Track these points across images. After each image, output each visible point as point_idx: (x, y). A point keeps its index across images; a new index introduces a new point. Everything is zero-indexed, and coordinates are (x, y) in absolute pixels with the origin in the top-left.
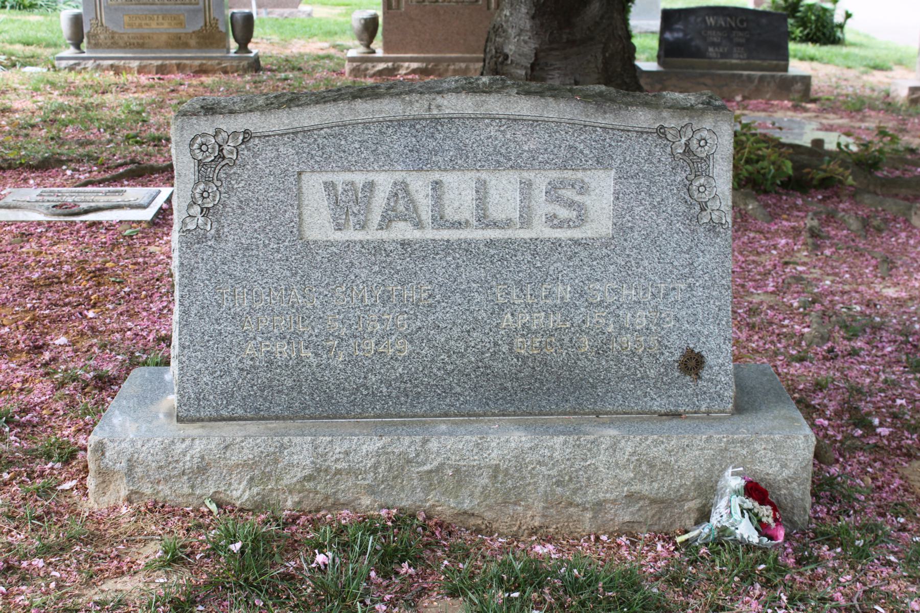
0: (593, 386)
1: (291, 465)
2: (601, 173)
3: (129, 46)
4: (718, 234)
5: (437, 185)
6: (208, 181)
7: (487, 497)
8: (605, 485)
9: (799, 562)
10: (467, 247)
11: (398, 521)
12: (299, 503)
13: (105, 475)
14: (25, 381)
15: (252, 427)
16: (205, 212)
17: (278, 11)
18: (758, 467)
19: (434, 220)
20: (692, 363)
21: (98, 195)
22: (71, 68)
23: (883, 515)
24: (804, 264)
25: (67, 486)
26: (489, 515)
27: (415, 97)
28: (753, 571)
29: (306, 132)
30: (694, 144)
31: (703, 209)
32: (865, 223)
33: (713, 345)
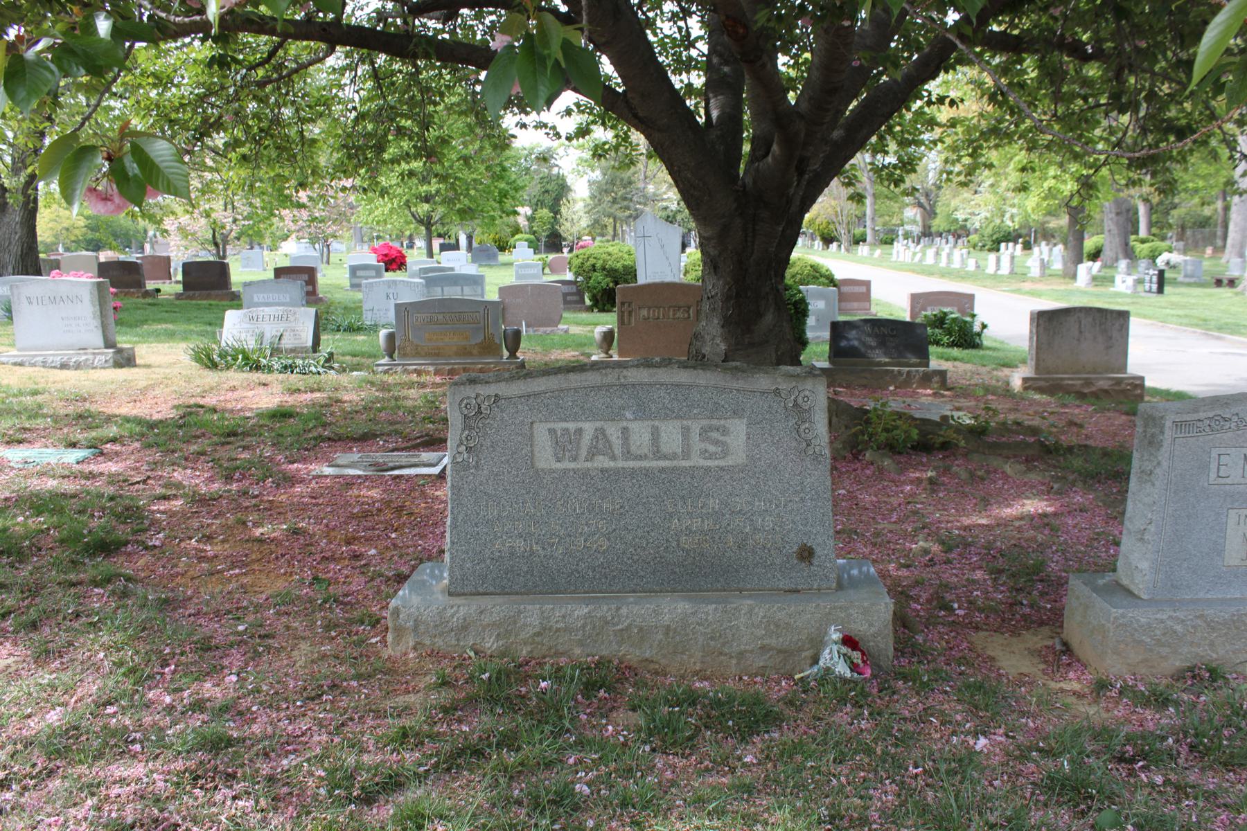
0: (737, 571)
1: (525, 625)
2: (737, 421)
3: (428, 355)
4: (820, 463)
5: (625, 430)
6: (471, 428)
7: (662, 648)
8: (745, 640)
9: (880, 691)
10: (646, 473)
11: (598, 664)
12: (531, 652)
13: (399, 631)
14: (347, 577)
15: (499, 599)
16: (469, 449)
17: (542, 329)
18: (853, 626)
19: (623, 454)
20: (806, 554)
21: (402, 457)
22: (386, 372)
23: (949, 664)
24: (922, 503)
25: (374, 641)
26: (663, 662)
27: (609, 371)
28: (847, 694)
29: (536, 395)
30: (800, 401)
31: (808, 445)
32: (972, 475)
33: (820, 540)
